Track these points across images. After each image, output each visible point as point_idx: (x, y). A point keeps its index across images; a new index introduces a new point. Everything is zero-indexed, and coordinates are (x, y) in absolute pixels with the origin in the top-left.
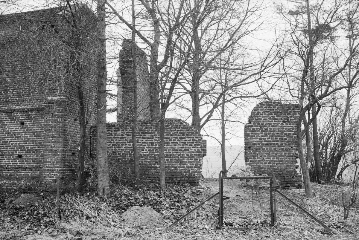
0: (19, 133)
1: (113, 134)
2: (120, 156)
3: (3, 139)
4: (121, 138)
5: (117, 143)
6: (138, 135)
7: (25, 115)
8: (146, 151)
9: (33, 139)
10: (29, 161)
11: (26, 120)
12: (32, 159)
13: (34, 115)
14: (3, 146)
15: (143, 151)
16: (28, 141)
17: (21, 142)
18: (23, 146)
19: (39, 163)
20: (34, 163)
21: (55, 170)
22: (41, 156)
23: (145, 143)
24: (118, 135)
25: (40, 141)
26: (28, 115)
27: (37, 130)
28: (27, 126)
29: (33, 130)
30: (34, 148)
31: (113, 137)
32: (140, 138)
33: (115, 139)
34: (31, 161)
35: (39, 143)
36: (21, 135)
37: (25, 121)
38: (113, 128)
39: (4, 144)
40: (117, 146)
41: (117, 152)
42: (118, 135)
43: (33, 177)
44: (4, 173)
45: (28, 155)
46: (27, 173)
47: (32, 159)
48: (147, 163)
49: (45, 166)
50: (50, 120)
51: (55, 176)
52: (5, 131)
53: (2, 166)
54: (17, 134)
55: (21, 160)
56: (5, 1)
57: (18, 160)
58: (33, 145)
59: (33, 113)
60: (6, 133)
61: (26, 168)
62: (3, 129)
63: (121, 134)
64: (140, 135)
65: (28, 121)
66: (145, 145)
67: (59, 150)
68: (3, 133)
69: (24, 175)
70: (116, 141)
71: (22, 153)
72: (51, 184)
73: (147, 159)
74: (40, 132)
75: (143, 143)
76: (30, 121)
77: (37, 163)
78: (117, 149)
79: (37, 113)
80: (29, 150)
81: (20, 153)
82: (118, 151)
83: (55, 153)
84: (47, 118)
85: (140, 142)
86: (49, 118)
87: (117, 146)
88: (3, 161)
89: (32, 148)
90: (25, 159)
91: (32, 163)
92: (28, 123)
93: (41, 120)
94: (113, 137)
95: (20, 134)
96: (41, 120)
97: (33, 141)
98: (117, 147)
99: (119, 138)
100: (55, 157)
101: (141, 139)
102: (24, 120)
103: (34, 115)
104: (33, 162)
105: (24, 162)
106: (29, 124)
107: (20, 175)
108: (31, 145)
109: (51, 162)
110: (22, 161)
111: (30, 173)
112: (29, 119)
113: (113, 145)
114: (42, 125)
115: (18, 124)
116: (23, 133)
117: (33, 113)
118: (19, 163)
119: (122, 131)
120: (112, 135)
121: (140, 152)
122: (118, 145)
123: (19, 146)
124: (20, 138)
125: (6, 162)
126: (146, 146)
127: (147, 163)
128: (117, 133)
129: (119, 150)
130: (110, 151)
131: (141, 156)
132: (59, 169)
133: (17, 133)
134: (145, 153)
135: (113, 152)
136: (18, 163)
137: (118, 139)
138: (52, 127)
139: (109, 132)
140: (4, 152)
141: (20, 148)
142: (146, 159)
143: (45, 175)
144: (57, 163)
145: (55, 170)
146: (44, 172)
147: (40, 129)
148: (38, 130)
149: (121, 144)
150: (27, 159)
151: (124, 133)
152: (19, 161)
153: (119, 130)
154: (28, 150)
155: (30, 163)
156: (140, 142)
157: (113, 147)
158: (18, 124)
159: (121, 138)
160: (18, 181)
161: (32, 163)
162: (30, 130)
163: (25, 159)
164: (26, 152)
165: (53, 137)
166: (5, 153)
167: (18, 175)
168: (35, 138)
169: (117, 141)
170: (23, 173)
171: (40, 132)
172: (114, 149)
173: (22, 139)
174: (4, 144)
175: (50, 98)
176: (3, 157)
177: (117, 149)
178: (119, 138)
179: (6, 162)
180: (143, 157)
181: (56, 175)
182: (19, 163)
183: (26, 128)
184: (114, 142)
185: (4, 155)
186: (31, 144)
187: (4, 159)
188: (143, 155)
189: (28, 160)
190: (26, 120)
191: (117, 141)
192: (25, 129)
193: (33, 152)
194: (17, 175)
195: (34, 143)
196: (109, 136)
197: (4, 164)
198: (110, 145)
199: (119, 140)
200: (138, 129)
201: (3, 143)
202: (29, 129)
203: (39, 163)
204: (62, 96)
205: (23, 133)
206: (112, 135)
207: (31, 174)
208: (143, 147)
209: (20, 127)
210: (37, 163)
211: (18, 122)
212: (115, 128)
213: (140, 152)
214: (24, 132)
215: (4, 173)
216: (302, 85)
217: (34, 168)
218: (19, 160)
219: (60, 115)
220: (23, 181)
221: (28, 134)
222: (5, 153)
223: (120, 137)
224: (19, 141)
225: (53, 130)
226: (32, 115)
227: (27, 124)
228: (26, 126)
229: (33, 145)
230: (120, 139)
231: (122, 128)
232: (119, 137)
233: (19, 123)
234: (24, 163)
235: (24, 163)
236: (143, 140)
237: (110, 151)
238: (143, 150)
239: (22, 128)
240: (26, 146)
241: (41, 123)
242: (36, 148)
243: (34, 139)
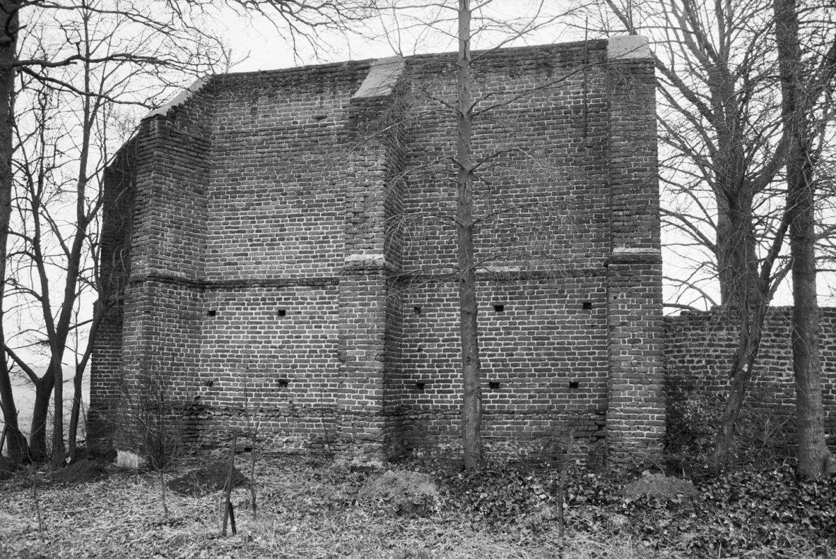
0: (490, 330)
1: (708, 338)
2: (726, 388)
3: (446, 343)
4: (726, 346)
5: (717, 357)
6: (767, 341)
7: (506, 289)
8: (788, 378)
9: (529, 344)
10: (519, 397)
11: (508, 301)
12: (529, 391)
13: (530, 288)
14: (448, 361)
15: (781, 378)
16: (516, 349)
17: (497, 350)
18: (502, 361)
19: (548, 402)
20: (534, 402)
21: (647, 418)
22: (552, 385)
23: (784, 358)
24: (720, 340)
25: (550, 349)
26: (513, 288)
27: (539, 323)
28: (513, 313)
29: (529, 323)
30: (533, 365)
31: (706, 342)
32: (773, 347)
33: (713, 349)
34: (525, 397)
35: (545, 354)
36: (496, 335)
37: (506, 303)
38: (707, 323)
39: (449, 356)
40: (718, 364)
41: (718, 378)
42: (720, 340)
43: (534, 434)
44: (454, 423)
45: (517, 381)
46: (518, 423)
47: (529, 391)
48: (791, 404)
49: (617, 408)
50: (624, 301)
51: (645, 433)
52: (452, 325)
53: (446, 407)
54: (484, 332)
55: (498, 394)
56: (575, 5)
57: (489, 394)
58: (529, 360)
59: (528, 284)
60: (453, 330)
61: (513, 413)
62: (446, 320)
63: (726, 337)
64: (772, 341)
65: (513, 303)
66: (785, 364)
67: (651, 372)
68: (447, 330)
69: (508, 428)
70: (715, 354)
71: (500, 376)
72: (636, 451)
73: (791, 396)
74: (549, 328)
75: (779, 358)
76: (519, 303)
77: (544, 402)
78: (718, 371)
79: (538, 284)
80: (520, 370)
81: (494, 376)
82: (720, 377)
83: (640, 379)
84: (615, 298)
85: (773, 357)
86: (622, 296)
87: (718, 364)
88: (449, 395)
89: (528, 365)
90: (510, 391)
91: (528, 402)
92: (513, 307)
93: (549, 302)
94: (706, 342)
95: (494, 332)
96: (549, 302)
97: (530, 349)
98: (718, 367)
99: (721, 346)
100: (640, 388)
101: (776, 350)
102: (502, 299)
103: (530, 288)
104: (531, 400)
105: (507, 399)
106: (516, 309)
107: (497, 429)
108: (524, 360)
109: (631, 400)
110: (501, 396)
111: (526, 423)
112: (517, 298)
113: (708, 362)
114: (553, 312)
115: (488, 309)
116: (502, 331)
117: (528, 284)
118: (494, 402)
119: (727, 330)
120: (704, 339)
121: (773, 379)
122: (721, 363)
123: (491, 360)
124: (493, 342)
125: (456, 397)
126: (787, 366)
127: (791, 404)
128: (716, 335)
129: (723, 373)
130: (702, 375)
131: (777, 388)
132: (656, 415)
133: (485, 329)
134: (787, 381)
135: (708, 378)
136: (491, 400)
137: (719, 349)
138: (630, 319)
139: (698, 331)
140: (450, 374)
141: (494, 366)
142: (788, 394)
143: (619, 429)
144: (646, 401)
145: (647, 418)
146: (619, 423)
147: (548, 323)
148: (544, 323)
149: (726, 360)
150: (515, 391)
151: (734, 335)
152: (491, 397)
153: (720, 329)
154: (515, 370)
155: (523, 402)
156: (773, 357)
157: (708, 366)
158: (488, 309)
159: (726, 346)
160: (491, 443)
161: (528, 402)
162: (520, 323)
163: (510, 391)
164: (511, 376)
165: (634, 341)
166: (452, 377)
167: (493, 429)
168: (536, 342)
169: (717, 353)
170: (507, 423)
171: (549, 328)
172: (710, 371)
173: (500, 345)
174: (449, 356)
175: (354, 257)
176: (449, 386)
177: (718, 371)
178: (721, 346)
179: (456, 397)
180: (780, 391)
181: (649, 429)
182: (494, 402)
183: (508, 318)
184: (709, 356)
185: (450, 381)
186: (525, 357)
187: (452, 392)
188: (782, 386)
189: (518, 394)
190: (508, 301)
191: (717, 353)
192: (508, 321)
193: (530, 376)
194: (489, 429)
195: (532, 354)
196: (697, 340)
197: (451, 402)
198: (699, 362)
199: (722, 351)
200: (766, 327)
201: (447, 354)
202: (518, 321)
203: (548, 402)
204: (649, 247)
205: (502, 331)
206: (704, 339)
207: (528, 426)
208: (781, 368)
209: (492, 317)
210: (544, 402)
211: (487, 304)
212: (711, 324)
213: (773, 379)
214: (504, 328)
215: (454, 423)
216: (123, 281)
217: (535, 412)
218: (493, 393)
219: (650, 290)
220: (507, 443)
221: (516, 334)
222: (452, 377)
223: (723, 343)
224: (491, 350)
225: (633, 325)
226: (524, 288)
227: (511, 308)
228: (508, 314)
229: (529, 360)
230: (723, 349)
231: (727, 324)
232: (721, 343)
233: (488, 306)
234: (507, 402)
235: (507, 402)
236: (779, 353)
237: (702, 375)
238: (781, 375)
239: (498, 319)
240: (510, 360)
241: (550, 307)
242: (540, 367)
243: (533, 344)
